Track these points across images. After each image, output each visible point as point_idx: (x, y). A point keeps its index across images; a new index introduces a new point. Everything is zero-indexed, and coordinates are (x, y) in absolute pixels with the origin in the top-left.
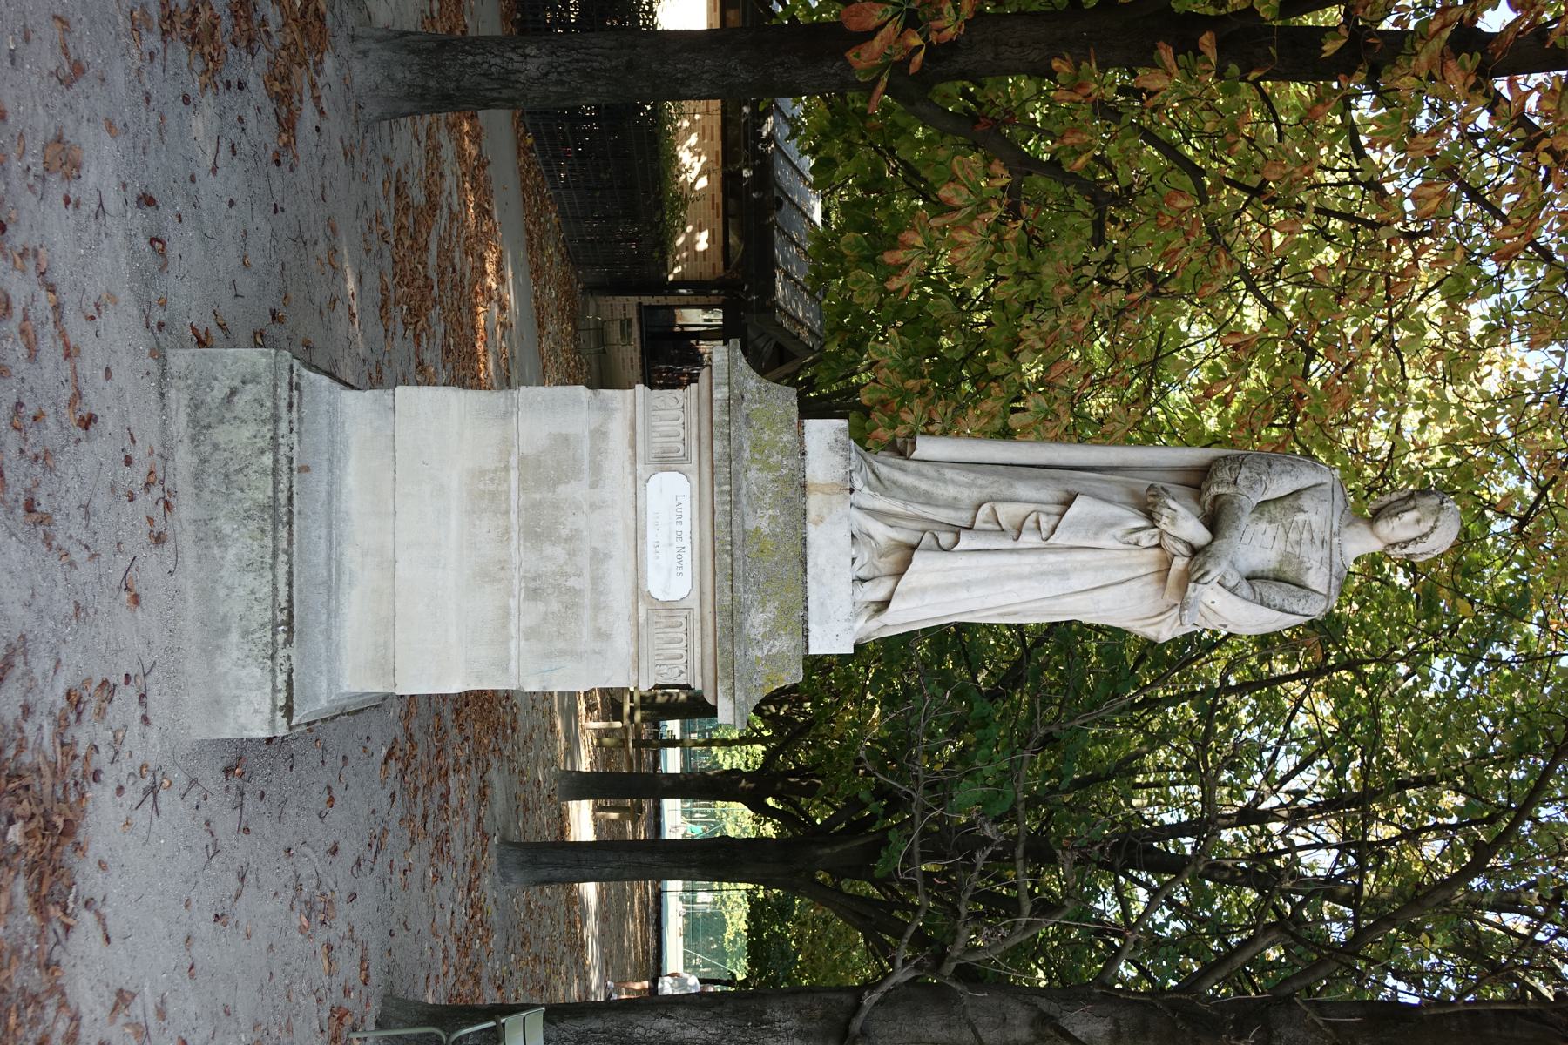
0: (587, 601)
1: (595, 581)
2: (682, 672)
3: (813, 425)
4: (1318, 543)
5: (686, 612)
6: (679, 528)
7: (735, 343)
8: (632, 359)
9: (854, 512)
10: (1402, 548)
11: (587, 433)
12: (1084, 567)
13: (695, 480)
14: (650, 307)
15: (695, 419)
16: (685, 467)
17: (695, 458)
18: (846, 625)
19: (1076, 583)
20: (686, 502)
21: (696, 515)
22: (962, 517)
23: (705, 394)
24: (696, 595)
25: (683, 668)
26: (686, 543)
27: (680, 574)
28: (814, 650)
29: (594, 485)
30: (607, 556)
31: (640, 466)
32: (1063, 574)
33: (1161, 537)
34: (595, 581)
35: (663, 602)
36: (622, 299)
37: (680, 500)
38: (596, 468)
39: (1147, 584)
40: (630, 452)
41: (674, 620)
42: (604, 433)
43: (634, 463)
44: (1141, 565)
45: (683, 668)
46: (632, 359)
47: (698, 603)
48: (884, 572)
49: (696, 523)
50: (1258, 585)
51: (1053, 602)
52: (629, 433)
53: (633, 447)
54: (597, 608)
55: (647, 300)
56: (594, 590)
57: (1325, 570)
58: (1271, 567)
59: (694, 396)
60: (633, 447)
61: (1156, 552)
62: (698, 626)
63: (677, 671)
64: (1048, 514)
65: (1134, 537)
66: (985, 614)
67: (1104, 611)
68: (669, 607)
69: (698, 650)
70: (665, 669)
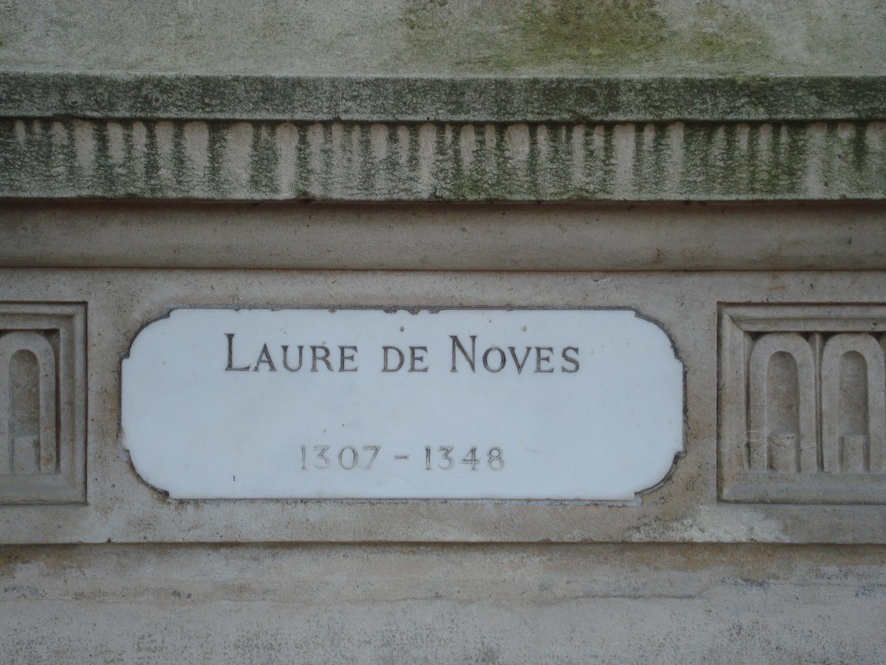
5: (734, 337)
35: (689, 433)
41: (763, 387)
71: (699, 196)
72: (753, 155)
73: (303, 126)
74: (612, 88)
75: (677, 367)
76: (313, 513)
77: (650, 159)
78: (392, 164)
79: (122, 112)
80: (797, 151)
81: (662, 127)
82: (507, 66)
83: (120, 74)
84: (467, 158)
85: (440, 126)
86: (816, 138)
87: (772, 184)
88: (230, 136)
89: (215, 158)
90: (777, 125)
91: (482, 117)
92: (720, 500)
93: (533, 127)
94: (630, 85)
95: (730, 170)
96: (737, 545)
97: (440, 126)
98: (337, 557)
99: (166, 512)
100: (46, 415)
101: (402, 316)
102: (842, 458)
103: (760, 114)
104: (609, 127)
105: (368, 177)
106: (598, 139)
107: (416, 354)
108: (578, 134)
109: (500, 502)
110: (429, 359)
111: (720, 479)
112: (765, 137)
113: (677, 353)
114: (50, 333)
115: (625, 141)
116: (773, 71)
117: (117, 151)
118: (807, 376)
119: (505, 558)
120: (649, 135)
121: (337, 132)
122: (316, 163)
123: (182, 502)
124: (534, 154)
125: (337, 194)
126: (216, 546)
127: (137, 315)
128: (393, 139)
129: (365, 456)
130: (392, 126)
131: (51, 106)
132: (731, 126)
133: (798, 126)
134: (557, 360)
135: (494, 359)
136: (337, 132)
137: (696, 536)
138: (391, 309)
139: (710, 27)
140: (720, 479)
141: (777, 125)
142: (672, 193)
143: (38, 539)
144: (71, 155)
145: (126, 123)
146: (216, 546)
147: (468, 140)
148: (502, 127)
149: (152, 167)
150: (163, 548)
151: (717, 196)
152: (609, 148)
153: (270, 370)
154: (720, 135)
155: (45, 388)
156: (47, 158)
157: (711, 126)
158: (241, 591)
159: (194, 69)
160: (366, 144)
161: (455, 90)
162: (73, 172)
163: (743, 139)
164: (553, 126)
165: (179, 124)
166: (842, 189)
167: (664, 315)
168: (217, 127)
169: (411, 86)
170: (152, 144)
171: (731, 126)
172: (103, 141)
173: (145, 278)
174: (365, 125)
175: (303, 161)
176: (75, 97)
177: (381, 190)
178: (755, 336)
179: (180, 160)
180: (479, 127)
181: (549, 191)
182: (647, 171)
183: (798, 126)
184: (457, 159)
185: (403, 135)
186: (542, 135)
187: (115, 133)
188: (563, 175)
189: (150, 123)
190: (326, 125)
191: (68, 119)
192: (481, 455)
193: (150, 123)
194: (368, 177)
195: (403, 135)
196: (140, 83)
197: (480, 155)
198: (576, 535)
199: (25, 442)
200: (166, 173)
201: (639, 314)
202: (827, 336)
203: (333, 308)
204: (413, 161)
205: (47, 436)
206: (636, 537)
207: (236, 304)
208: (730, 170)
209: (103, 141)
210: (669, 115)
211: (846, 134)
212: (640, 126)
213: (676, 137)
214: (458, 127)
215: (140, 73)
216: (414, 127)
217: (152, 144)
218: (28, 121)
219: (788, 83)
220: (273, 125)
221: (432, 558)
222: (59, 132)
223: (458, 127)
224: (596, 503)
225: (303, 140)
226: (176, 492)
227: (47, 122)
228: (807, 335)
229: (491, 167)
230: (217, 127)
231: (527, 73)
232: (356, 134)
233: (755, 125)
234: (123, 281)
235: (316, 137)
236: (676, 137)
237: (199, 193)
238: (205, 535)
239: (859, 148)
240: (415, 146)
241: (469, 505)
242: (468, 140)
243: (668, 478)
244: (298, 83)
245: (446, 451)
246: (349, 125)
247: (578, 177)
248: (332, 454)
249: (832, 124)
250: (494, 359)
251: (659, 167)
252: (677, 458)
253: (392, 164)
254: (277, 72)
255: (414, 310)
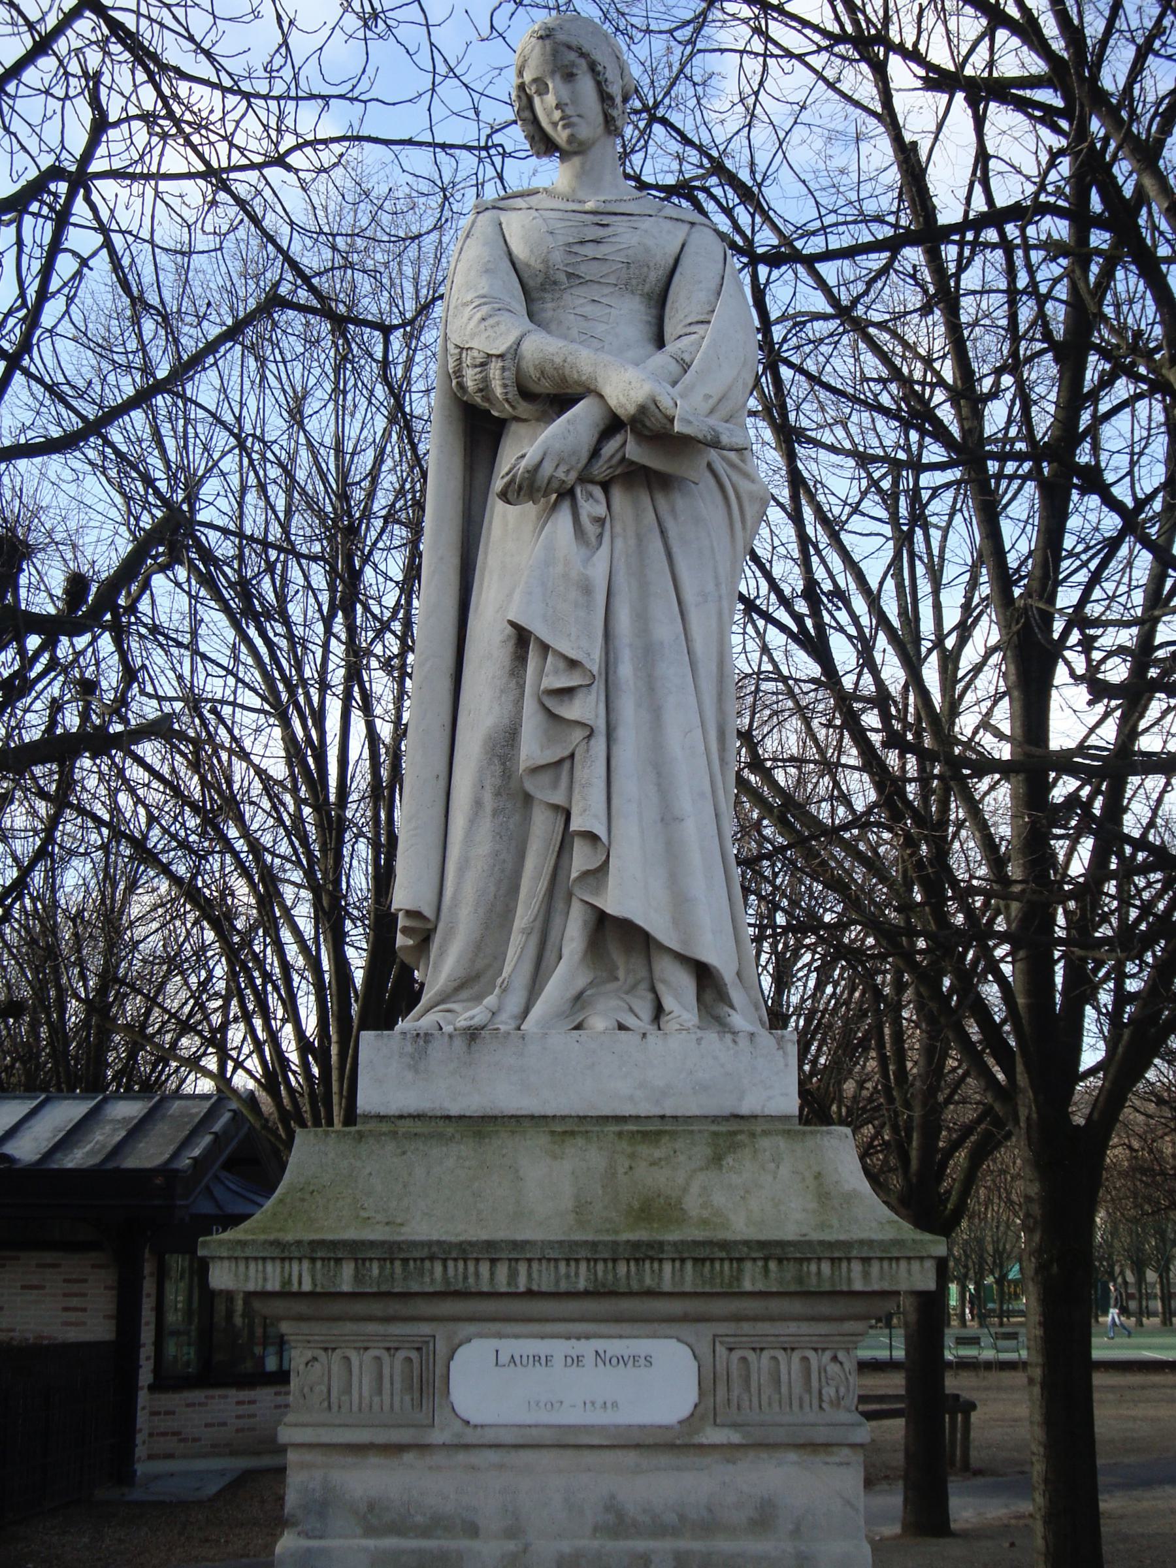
0: (697, 1545)
1: (659, 1530)
2: (835, 1359)
3: (368, 1099)
4: (600, 232)
5: (721, 1350)
6: (558, 1360)
7: (205, 1243)
8: (239, 1403)
9: (529, 1025)
10: (613, 105)
11: (371, 1543)
12: (642, 618)
13: (471, 1328)
14: (157, 1370)
15: (350, 1327)
16: (441, 1347)
17: (425, 1329)
18: (743, 1042)
19: (666, 629)
20: (509, 1347)
21: (535, 1328)
22: (542, 826)
23: (301, 1307)
24: (686, 1330)
25: (828, 1355)
26: (586, 1348)
27: (648, 1360)
28: (789, 1103)
29: (473, 1530)
30: (612, 1506)
31: (437, 1437)
32: (648, 654)
33: (593, 482)
34: (659, 1530)
35: (701, 1393)
36: (142, 1419)
37: (504, 1358)
38: (437, 1525)
39: (673, 511)
40: (409, 1457)
41: (735, 1373)
42: (371, 1506)
43: (423, 1448)
44: (638, 518)
45: (828, 1355)
46: (239, 1403)
47: (701, 1327)
48: (643, 973)
49: (549, 1328)
50: (670, 330)
51: (702, 671)
52: (374, 1459)
53: (399, 1449)
54: (709, 1526)
55: (145, 1376)
56: (674, 1531)
57: (646, 224)
58: (642, 308)
59: (305, 1327)
60: (399, 1449)
61: (617, 494)
62: (746, 1327)
63: (833, 1368)
64: (541, 672)
65: (591, 529)
66: (721, 792)
67: (718, 585)
68: (708, 1384)
69: (793, 1328)
70: (829, 1392)
71: (699, 1290)
72: (722, 1272)
73: (529, 1260)
74: (661, 1244)
75: (695, 1364)
76: (534, 1431)
77: (678, 1274)
78: (568, 1276)
79: (454, 1255)
80: (740, 1270)
81: (683, 1260)
82: (616, 1232)
83: (453, 1239)
84: (600, 1274)
85: (588, 1260)
86: (748, 1265)
87: (730, 1285)
88: (499, 1265)
89: (492, 1274)
90: (731, 1260)
91: (606, 1256)
92: (715, 1424)
93: (628, 1260)
94: (669, 1243)
95: (712, 1278)
96: (722, 1445)
97: (588, 1260)
98: (544, 1452)
99: (469, 1430)
100: (416, 1386)
101: (573, 1341)
102: (770, 1404)
103: (723, 1255)
104: (661, 1260)
105: (557, 1282)
106: (656, 1265)
107: (578, 1360)
108: (647, 1264)
109: (617, 1427)
110: (585, 1361)
111: (715, 1415)
112: (726, 1265)
113: (695, 1357)
114: (419, 1349)
115: (667, 1267)
116: (729, 1236)
117: (451, 1271)
118: (754, 1367)
119: (619, 1453)
120: (677, 1264)
121: (544, 1263)
122: (535, 1275)
123: (476, 1426)
124: (628, 1271)
125: (544, 1289)
126: (491, 1446)
127: (457, 1341)
128: (568, 1265)
129: (557, 1405)
130: (568, 1260)
131: (425, 1253)
132: (712, 1260)
133: (740, 1260)
134: (642, 1361)
135: (614, 1361)
136: (544, 1263)
137: (705, 1441)
138: (568, 1338)
139: (706, 1214)
140: (715, 1415)
141: (731, 1260)
142: (688, 1288)
143: (412, 1441)
144: (432, 1273)
145: (455, 1260)
146: (491, 1446)
147: (600, 1266)
148: (615, 1260)
149: (465, 1278)
150: (467, 1447)
151: (707, 1289)
152: (661, 1270)
153: (613, 1497)
154: (708, 1264)
155: (416, 1373)
156: (422, 1274)
157: (703, 1260)
158: (501, 1467)
159: (484, 1236)
160: (556, 1268)
161: (594, 1245)
162: (433, 1281)
163: (717, 1265)
164: (637, 1260)
165: (477, 1260)
166: (760, 1286)
167: (691, 1340)
168: (493, 1261)
169: (576, 1243)
170: (466, 1268)
171: (712, 1260)
172: (445, 1268)
173: (461, 1325)
174: (556, 1260)
175: (529, 1275)
176: (435, 1249)
177: (563, 1286)
178: (731, 1350)
179: (477, 1275)
180: (605, 1260)
181: (635, 1287)
182: (677, 1279)
183: (740, 1260)
184: (596, 1274)
185: (573, 1264)
186: (632, 1264)
187: (451, 1264)
188: (641, 1281)
189: (465, 1260)
190: (540, 1260)
191: (432, 1258)
192: (609, 1405)
193: (465, 1260)
194: (557, 1282)
195: (573, 1264)
196: (461, 1244)
197: (605, 1271)
198: (651, 1441)
199: (407, 1398)
200: (471, 1280)
201: (679, 1340)
202: (762, 1349)
203: (542, 1338)
204: (577, 1274)
205: (416, 1395)
206: (678, 1442)
207: (500, 1336)
208: (712, 1278)
209: (445, 1268)
210: (686, 1255)
211: (760, 1263)
212: (673, 1260)
213: (689, 1265)
214: (596, 1260)
215: (461, 1238)
216: (577, 1260)
217: (466, 1268)
218: (415, 1260)
219: (736, 1243)
220: (517, 1260)
221: (586, 1452)
222: (427, 1264)
223: (596, 1260)
224: (660, 1427)
225: (530, 1266)
226: (473, 1421)
227: (422, 1260)
228: (754, 1349)
229: (610, 1277)
230: (493, 1261)
231: (625, 1236)
232: (552, 1264)
233: (722, 1260)
234: (451, 1326)
235: (535, 1265)
236: (689, 1265)
237: (485, 1289)
238: (485, 1441)
239: (766, 1269)
240: (577, 1268)
241: (603, 1428)
242: (600, 1266)
243: (692, 1415)
244: (527, 1242)
245: (593, 1403)
246: (549, 1260)
247: (648, 1281)
248: (542, 1404)
249: (754, 1260)
250: (614, 1361)
251: (682, 1277)
252: (696, 1406)
253: (568, 1276)
254: (520, 1237)
255: (578, 1338)
